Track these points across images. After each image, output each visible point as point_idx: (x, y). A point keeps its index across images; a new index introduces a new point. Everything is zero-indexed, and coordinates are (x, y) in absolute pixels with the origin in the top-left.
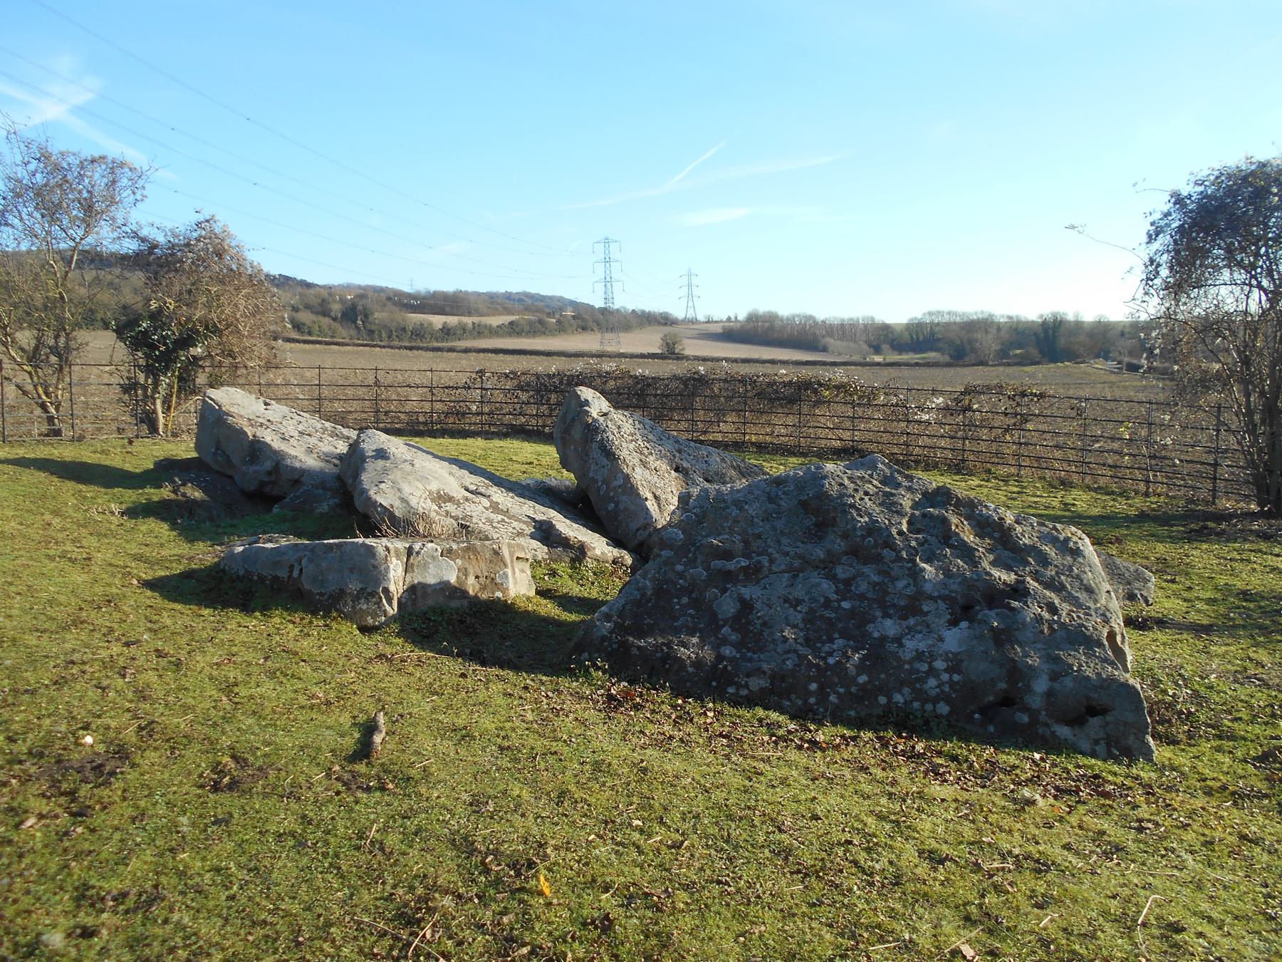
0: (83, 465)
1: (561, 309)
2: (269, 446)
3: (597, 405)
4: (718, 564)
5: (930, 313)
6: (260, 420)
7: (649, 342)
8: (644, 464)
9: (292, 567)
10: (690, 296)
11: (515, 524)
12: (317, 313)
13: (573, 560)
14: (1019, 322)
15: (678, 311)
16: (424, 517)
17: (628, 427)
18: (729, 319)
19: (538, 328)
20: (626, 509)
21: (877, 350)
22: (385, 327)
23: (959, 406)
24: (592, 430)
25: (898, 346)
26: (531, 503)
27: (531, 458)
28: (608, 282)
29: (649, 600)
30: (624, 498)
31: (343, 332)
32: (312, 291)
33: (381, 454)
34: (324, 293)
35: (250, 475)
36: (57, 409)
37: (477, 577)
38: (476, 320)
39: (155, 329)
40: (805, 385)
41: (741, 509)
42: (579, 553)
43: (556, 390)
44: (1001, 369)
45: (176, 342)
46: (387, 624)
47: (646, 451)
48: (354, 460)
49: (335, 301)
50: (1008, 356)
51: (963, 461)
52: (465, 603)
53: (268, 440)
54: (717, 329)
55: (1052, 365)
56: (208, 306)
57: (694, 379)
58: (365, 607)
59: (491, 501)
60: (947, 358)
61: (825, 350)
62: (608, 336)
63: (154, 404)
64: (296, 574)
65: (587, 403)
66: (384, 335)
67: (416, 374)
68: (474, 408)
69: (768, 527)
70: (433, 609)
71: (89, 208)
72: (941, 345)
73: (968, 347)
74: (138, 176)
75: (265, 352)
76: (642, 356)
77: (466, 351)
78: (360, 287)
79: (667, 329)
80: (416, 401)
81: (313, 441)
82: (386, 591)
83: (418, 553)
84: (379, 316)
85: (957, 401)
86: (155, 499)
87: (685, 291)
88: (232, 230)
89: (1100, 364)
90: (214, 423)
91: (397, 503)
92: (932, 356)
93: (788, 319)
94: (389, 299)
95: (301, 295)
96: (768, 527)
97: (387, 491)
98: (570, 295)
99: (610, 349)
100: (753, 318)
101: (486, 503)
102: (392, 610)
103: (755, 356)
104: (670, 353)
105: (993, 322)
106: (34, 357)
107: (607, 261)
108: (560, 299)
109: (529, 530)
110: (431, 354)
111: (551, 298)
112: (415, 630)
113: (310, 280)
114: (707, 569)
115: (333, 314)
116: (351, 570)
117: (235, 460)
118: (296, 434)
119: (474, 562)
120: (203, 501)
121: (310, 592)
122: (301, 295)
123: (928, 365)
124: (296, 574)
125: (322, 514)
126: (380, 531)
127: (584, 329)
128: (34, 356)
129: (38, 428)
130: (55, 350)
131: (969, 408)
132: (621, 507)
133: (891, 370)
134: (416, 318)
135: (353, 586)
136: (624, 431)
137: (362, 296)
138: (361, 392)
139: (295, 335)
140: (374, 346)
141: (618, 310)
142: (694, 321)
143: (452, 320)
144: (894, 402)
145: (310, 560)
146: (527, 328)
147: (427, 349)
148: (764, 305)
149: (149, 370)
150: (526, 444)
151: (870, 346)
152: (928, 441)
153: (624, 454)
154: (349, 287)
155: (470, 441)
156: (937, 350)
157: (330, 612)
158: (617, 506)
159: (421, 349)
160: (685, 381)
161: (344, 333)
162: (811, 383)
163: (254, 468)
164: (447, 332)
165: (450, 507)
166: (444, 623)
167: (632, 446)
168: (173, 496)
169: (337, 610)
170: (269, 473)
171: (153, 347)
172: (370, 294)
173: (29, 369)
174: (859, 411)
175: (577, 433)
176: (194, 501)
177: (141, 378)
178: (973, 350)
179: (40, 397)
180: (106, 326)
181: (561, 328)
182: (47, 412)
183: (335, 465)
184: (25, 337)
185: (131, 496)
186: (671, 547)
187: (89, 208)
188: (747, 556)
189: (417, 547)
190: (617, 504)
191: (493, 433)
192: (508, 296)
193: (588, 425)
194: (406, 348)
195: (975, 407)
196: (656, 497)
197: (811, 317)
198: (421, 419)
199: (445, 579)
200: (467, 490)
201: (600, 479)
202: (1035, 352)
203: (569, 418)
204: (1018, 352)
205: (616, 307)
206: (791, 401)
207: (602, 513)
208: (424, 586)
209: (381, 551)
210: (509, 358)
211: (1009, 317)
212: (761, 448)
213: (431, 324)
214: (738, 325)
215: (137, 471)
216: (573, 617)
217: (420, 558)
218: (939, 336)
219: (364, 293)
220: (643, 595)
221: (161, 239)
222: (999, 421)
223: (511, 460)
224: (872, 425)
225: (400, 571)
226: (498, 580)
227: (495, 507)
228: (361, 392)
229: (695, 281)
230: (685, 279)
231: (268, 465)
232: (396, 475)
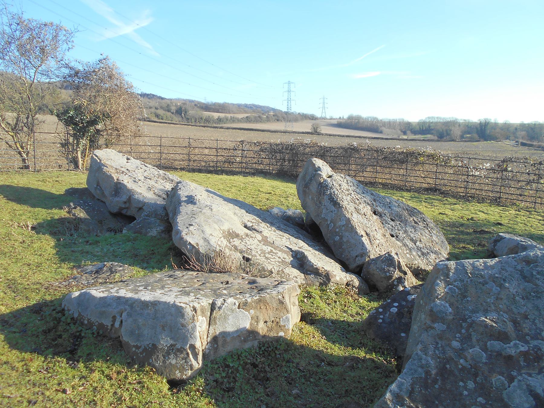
0: (28, 190)
1: (268, 112)
2: (125, 186)
3: (325, 170)
4: (496, 345)
5: (429, 118)
6: (123, 169)
7: (307, 127)
8: (357, 211)
9: (114, 318)
10: (324, 108)
11: (280, 254)
12: (165, 110)
13: (321, 284)
14: (469, 122)
15: (318, 114)
16: (220, 254)
17: (345, 186)
18: (340, 118)
19: (258, 120)
20: (348, 241)
21: (405, 133)
22: (193, 117)
23: (501, 167)
24: (323, 187)
25: (414, 132)
26: (286, 235)
27: (270, 189)
28: (289, 100)
29: (435, 381)
30: (347, 234)
31: (176, 119)
32: (164, 101)
33: (191, 200)
34: (169, 102)
35: (115, 203)
36: (27, 155)
37: (266, 322)
38: (232, 115)
39: (77, 115)
40: (411, 154)
41: (501, 286)
42: (327, 278)
43: (280, 152)
44: (462, 143)
45: (88, 122)
46: (193, 377)
47: (357, 202)
48: (172, 196)
49: (173, 105)
50: (463, 138)
51: (500, 198)
52: (256, 343)
53: (125, 182)
54: (335, 122)
55: (486, 142)
56: (105, 103)
57: (351, 149)
58: (174, 362)
59: (263, 236)
60: (436, 138)
61: (381, 132)
62: (288, 124)
63: (77, 153)
64: (117, 325)
65: (319, 169)
66: (193, 120)
67: (209, 140)
68: (238, 159)
69: (530, 306)
70: (231, 354)
71: (42, 50)
72: (433, 132)
73: (445, 133)
74: (69, 34)
75: (134, 128)
76: (303, 133)
77: (228, 128)
78: (184, 100)
79: (314, 121)
80: (210, 156)
81: (152, 183)
82: (193, 347)
83: (220, 308)
84: (191, 112)
85: (499, 166)
86: (56, 217)
87: (321, 105)
88: (118, 64)
89: (507, 142)
90: (96, 169)
91: (201, 243)
92: (429, 136)
93: (366, 119)
94: (196, 105)
95: (159, 102)
96: (530, 306)
97: (194, 232)
98: (272, 106)
99: (289, 129)
100: (350, 118)
101: (259, 237)
102: (197, 364)
103: (352, 134)
104: (315, 132)
105: (457, 122)
106: (15, 129)
107: (289, 91)
108: (268, 107)
109: (289, 259)
110: (213, 129)
111: (264, 107)
112: (216, 381)
113: (163, 96)
114: (485, 349)
115: (172, 111)
116: (163, 327)
117: (107, 193)
118: (142, 178)
119: (264, 310)
120: (86, 219)
121: (127, 343)
122: (159, 102)
123: (428, 140)
124: (117, 325)
125: (152, 237)
126: (189, 265)
127: (278, 120)
128: (15, 127)
129: (18, 163)
130: (26, 125)
131: (506, 170)
132: (345, 240)
133: (412, 142)
134: (206, 114)
135: (165, 342)
136: (342, 185)
137: (184, 104)
138: (180, 151)
139: (156, 120)
140: (189, 125)
141: (293, 113)
142: (325, 118)
143: (222, 115)
144: (460, 165)
145: (129, 315)
146: (253, 119)
147: (211, 127)
148: (356, 112)
149: (75, 136)
150: (265, 180)
151: (402, 131)
152: (477, 186)
153: (345, 204)
154: (178, 100)
155: (236, 177)
156: (432, 134)
157: (143, 366)
158: (341, 238)
159: (208, 127)
160: (345, 150)
161: (177, 119)
162: (414, 153)
163: (117, 199)
164: (220, 120)
165: (236, 242)
166: (240, 368)
167: (349, 198)
168: (67, 215)
169: (149, 364)
170: (125, 203)
171: (76, 124)
172: (188, 103)
173: (12, 134)
174: (440, 169)
175: (314, 188)
176: (80, 219)
177: (71, 140)
178: (448, 134)
179: (18, 149)
180: (52, 113)
181: (268, 120)
182: (22, 156)
183: (164, 199)
184: (10, 116)
185: (43, 214)
186: (443, 320)
187: (42, 50)
188: (522, 338)
189: (219, 302)
190: (341, 238)
191: (247, 173)
192: (246, 106)
193: (320, 184)
194: (202, 126)
195: (509, 169)
196: (367, 234)
197: (376, 118)
198: (212, 164)
199: (242, 326)
200: (246, 227)
201: (329, 219)
202: (476, 136)
203: (308, 178)
204: (468, 135)
205: (292, 111)
206: (402, 162)
207: (330, 242)
208: (224, 334)
209: (189, 311)
210: (246, 132)
211: (465, 120)
212: (385, 186)
213: (213, 117)
214: (344, 121)
215: (58, 193)
216: (337, 350)
217: (222, 311)
218: (432, 128)
219: (185, 102)
220: (428, 373)
221: (81, 68)
222: (525, 177)
223: (259, 190)
224: (447, 177)
225: (205, 326)
226: (282, 323)
227: (265, 241)
228: (180, 151)
229: (326, 101)
230: (322, 100)
231: (124, 198)
232: (200, 219)
